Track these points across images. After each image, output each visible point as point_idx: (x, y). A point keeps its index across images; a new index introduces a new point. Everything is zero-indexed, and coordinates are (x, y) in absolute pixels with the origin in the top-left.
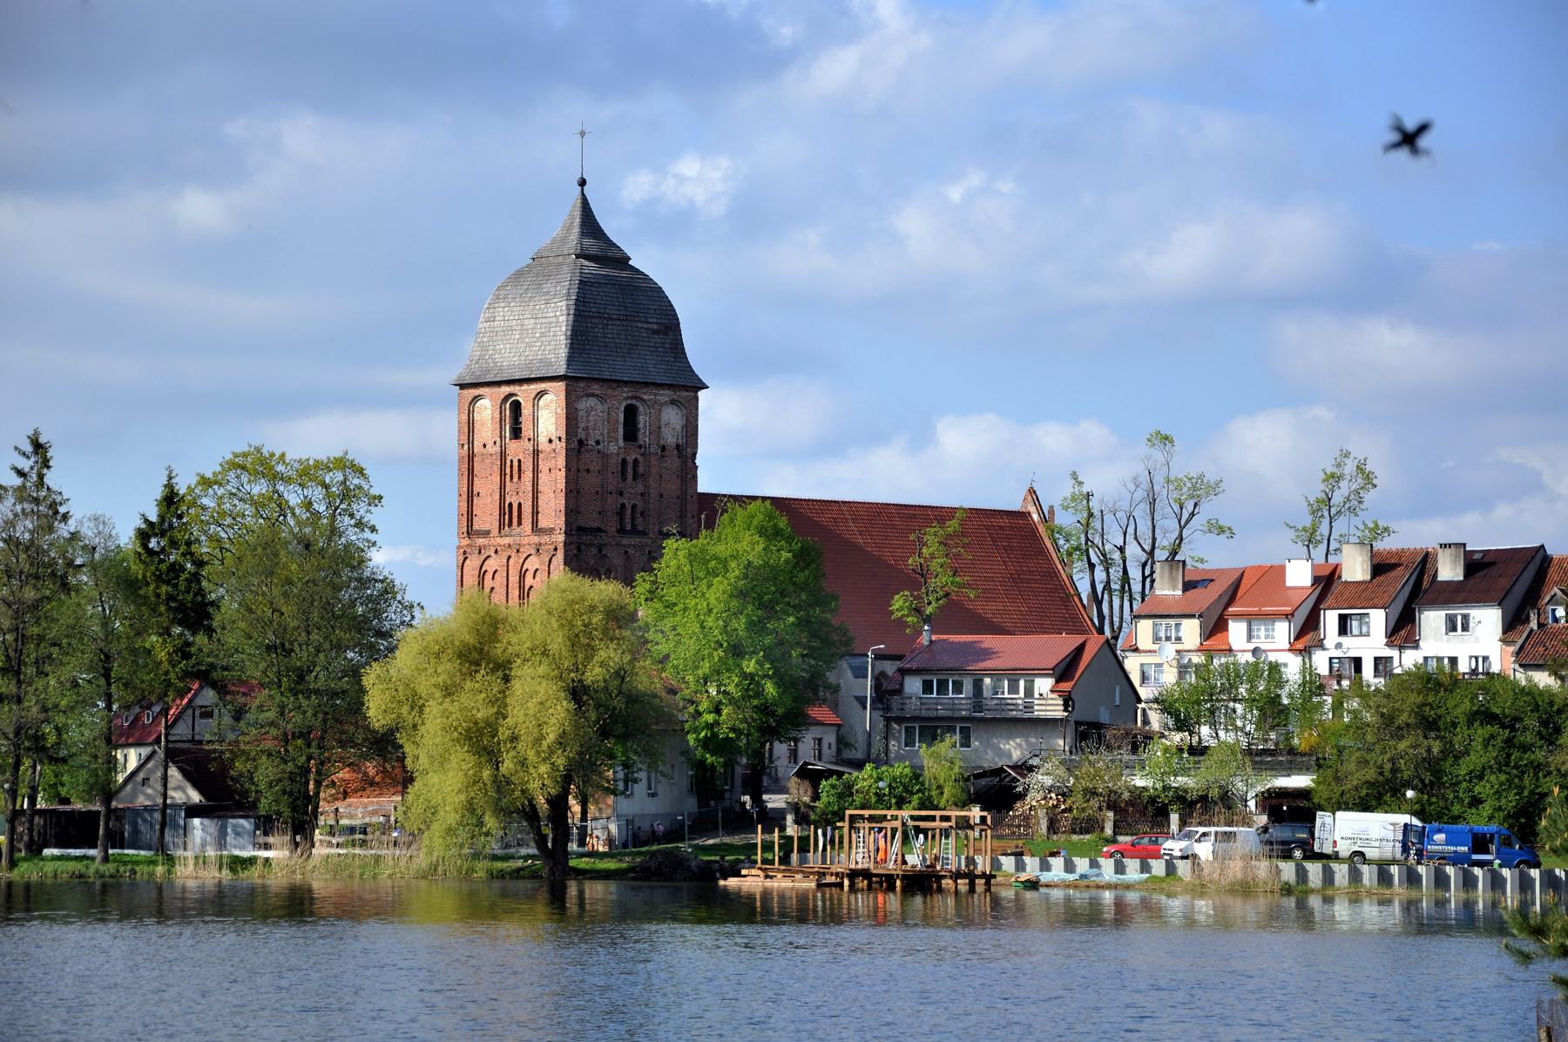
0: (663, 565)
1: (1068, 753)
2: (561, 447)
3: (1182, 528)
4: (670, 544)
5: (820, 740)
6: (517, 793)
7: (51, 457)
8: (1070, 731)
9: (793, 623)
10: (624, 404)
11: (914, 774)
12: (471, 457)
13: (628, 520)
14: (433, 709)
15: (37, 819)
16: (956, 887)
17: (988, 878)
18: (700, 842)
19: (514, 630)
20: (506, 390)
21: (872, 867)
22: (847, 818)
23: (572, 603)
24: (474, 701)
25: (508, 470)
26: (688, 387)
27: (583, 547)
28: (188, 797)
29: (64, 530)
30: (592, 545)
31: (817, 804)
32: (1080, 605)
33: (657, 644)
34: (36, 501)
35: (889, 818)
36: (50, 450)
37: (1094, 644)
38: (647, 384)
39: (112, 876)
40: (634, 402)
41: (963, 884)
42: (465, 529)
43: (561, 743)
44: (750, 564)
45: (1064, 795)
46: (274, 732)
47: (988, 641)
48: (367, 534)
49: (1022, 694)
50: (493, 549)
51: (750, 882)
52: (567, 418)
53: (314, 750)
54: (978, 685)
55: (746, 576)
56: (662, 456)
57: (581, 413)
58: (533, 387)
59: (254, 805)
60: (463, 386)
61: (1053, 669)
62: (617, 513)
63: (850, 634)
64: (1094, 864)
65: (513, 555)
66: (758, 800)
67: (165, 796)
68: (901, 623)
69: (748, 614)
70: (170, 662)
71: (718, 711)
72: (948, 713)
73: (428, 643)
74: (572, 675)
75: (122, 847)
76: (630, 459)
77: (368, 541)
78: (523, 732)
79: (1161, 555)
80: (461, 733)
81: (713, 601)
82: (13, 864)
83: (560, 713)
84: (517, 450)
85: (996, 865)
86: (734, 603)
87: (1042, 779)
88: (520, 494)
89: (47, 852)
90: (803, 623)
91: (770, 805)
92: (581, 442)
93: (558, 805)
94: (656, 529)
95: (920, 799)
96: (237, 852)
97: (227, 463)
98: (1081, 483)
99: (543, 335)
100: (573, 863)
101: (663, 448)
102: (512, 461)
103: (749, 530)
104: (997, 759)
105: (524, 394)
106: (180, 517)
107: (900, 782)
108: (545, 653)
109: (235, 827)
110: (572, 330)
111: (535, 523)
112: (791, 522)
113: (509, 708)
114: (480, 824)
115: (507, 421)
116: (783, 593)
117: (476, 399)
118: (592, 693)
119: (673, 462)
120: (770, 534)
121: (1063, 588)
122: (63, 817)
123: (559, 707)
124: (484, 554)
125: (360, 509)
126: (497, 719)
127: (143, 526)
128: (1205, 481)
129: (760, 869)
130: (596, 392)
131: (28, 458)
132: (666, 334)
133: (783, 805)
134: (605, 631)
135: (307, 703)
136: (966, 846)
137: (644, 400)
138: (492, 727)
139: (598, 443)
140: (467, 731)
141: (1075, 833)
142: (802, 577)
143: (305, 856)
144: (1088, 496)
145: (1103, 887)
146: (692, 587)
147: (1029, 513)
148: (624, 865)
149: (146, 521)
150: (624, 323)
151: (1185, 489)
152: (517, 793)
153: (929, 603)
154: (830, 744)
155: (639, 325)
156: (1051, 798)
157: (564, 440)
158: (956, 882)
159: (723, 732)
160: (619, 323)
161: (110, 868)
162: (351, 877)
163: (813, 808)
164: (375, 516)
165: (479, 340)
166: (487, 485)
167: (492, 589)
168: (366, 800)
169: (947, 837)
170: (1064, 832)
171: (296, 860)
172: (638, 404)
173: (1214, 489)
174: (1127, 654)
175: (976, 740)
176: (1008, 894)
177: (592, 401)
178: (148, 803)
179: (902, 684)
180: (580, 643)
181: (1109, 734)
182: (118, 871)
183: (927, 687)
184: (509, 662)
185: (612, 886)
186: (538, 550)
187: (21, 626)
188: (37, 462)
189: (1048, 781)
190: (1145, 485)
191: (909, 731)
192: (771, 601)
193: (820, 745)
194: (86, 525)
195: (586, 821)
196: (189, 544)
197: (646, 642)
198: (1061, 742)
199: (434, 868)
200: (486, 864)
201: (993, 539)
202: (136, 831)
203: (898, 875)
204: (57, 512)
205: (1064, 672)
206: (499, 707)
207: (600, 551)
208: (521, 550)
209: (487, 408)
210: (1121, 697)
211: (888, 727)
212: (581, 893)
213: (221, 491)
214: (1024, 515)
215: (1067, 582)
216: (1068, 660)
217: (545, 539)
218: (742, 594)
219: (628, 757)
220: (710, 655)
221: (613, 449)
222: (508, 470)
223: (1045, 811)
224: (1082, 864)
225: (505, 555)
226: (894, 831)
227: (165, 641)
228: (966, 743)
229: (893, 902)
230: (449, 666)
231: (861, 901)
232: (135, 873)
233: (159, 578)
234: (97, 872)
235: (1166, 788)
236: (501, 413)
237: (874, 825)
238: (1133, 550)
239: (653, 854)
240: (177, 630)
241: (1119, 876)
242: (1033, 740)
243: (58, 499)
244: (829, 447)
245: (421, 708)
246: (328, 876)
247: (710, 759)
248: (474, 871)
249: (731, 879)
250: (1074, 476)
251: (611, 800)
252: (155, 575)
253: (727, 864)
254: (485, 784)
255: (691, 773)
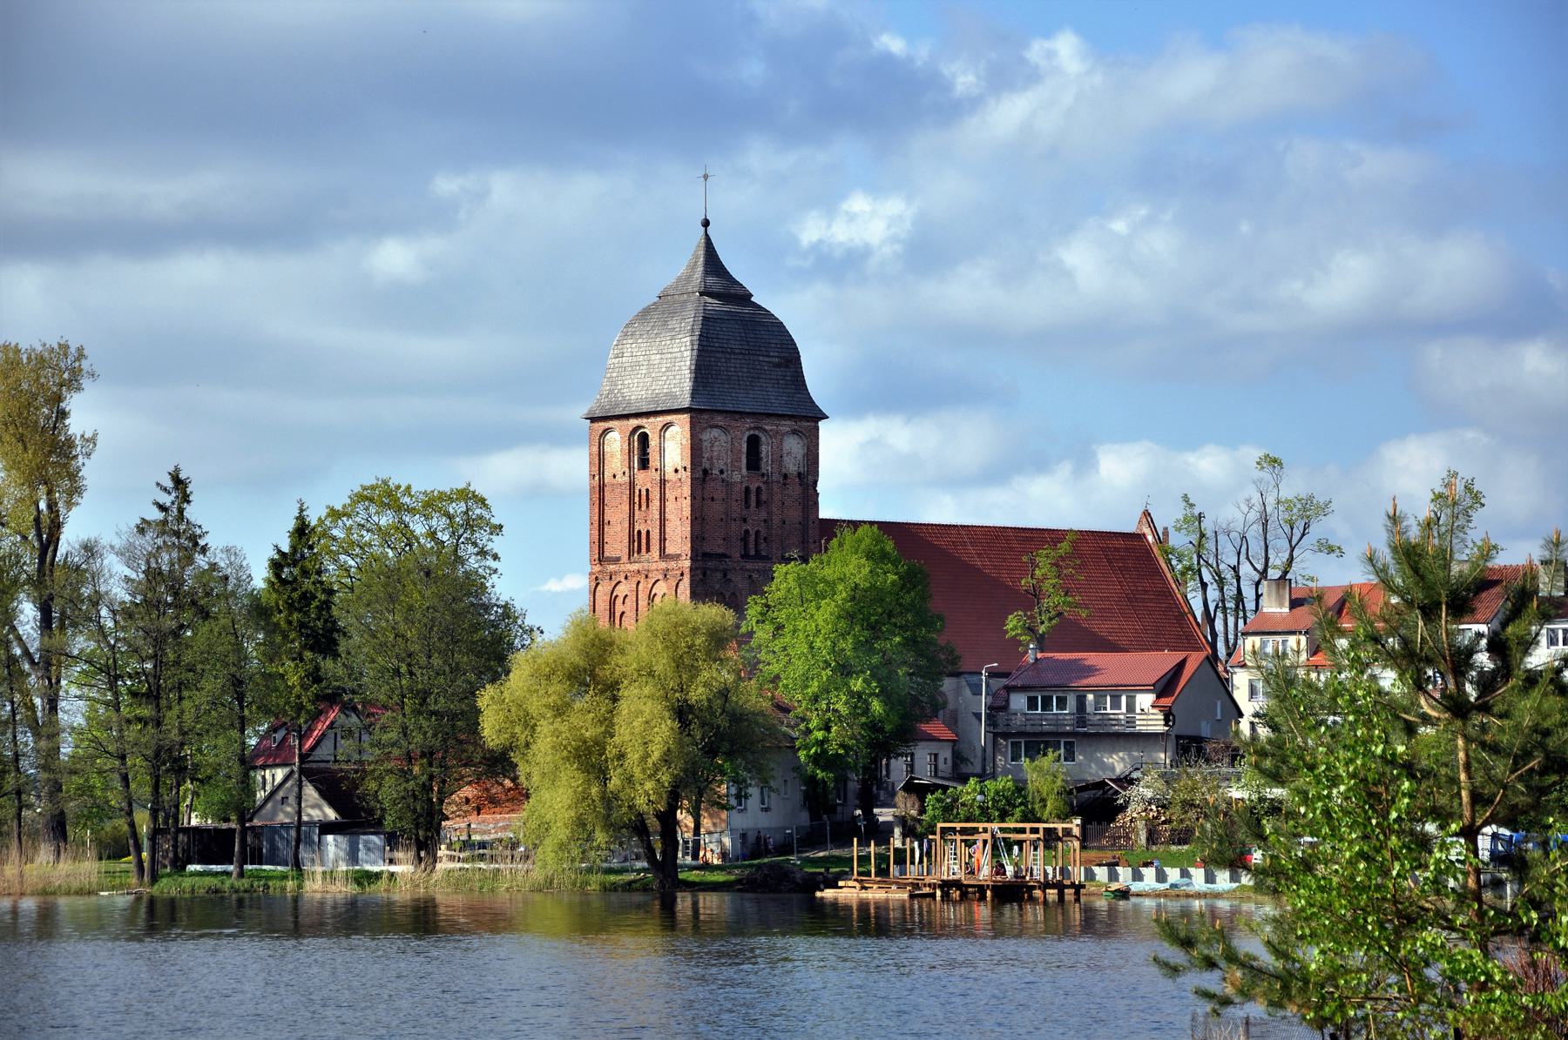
0: (774, 588)
1: (1169, 766)
2: (686, 476)
3: (1292, 551)
4: (780, 570)
5: (936, 755)
6: (624, 810)
7: (191, 492)
8: (1171, 746)
9: (899, 642)
10: (747, 434)
11: (1017, 787)
12: (602, 487)
13: (752, 546)
14: (544, 728)
15: (181, 836)
16: (1045, 897)
17: (1078, 888)
18: (811, 855)
19: (622, 652)
20: (634, 422)
21: (963, 879)
22: (938, 831)
23: (676, 625)
24: (583, 720)
25: (637, 499)
26: (808, 417)
27: (708, 572)
28: (325, 815)
29: (201, 561)
30: (717, 570)
31: (923, 817)
32: (1194, 623)
33: (769, 664)
34: (177, 534)
35: (981, 830)
36: (190, 486)
37: (1195, 660)
38: (769, 415)
39: (246, 891)
40: (756, 432)
41: (1052, 894)
42: (597, 556)
43: (666, 761)
44: (856, 585)
45: (1164, 806)
46: (396, 752)
47: (1092, 658)
48: (490, 562)
49: (1124, 709)
50: (623, 575)
51: (847, 893)
52: (692, 448)
53: (435, 770)
54: (1081, 701)
55: (853, 598)
56: (784, 484)
57: (705, 444)
58: (600, 424)
59: (379, 823)
60: (593, 420)
61: (1153, 685)
62: (741, 539)
63: (956, 653)
64: (1185, 874)
65: (642, 581)
66: (868, 814)
67: (299, 813)
68: (1015, 642)
69: (854, 635)
70: (302, 686)
71: (828, 729)
72: (1052, 729)
73: (540, 665)
74: (677, 695)
75: (261, 864)
76: (753, 487)
77: (489, 568)
78: (629, 750)
79: (1274, 574)
80: (570, 752)
81: (821, 623)
82: (155, 879)
83: (664, 731)
84: (644, 480)
85: (1090, 876)
86: (842, 624)
87: (1144, 791)
88: (648, 522)
89: (191, 868)
90: (911, 643)
91: (881, 819)
92: (705, 472)
93: (668, 822)
94: (779, 554)
95: (1023, 811)
96: (368, 867)
97: (356, 495)
98: (1192, 505)
99: (668, 369)
100: (682, 876)
101: (785, 476)
102: (640, 491)
103: (856, 553)
104: (1101, 773)
105: (651, 426)
106: (311, 547)
107: (1003, 795)
108: (651, 674)
109: (366, 842)
110: (696, 365)
111: (662, 549)
112: (898, 545)
113: (616, 727)
114: (589, 839)
115: (636, 453)
116: (890, 615)
117: (606, 431)
118: (697, 712)
119: (795, 490)
120: (877, 557)
121: (1177, 606)
122: (205, 835)
123: (663, 726)
124: (615, 579)
125: (482, 537)
126: (604, 737)
127: (276, 557)
128: (1315, 502)
129: (856, 880)
130: (720, 424)
131: (169, 493)
132: (787, 367)
133: (890, 818)
134: (708, 653)
135: (428, 724)
136: (1055, 857)
137: (766, 431)
138: (600, 745)
139: (722, 472)
140: (576, 749)
141: (1173, 844)
142: (907, 599)
143: (428, 871)
144: (1200, 517)
145: (1192, 896)
146: (801, 609)
147: (1144, 535)
148: (732, 878)
149: (279, 551)
150: (747, 357)
151: (1295, 510)
152: (624, 810)
153: (1042, 623)
154: (946, 759)
155: (761, 358)
156: (1151, 810)
157: (689, 470)
158: (1044, 892)
159: (833, 748)
160: (741, 357)
161: (245, 883)
162: (471, 890)
163: (920, 821)
164: (496, 544)
165: (609, 375)
166: (617, 514)
167: (623, 613)
168: (498, 816)
169: (1035, 849)
170: (1162, 843)
171: (420, 874)
172: (761, 435)
173: (1324, 509)
174: (1236, 670)
175: (1080, 754)
176: (1101, 904)
177: (716, 432)
178: (287, 821)
179: (1007, 701)
180: (685, 665)
181: (1208, 748)
182: (252, 886)
183: (1032, 703)
184: (617, 683)
185: (727, 897)
186: (665, 575)
187: (159, 653)
188: (177, 497)
189: (1149, 794)
190: (1258, 507)
191: (1015, 745)
192: (876, 621)
193: (936, 760)
194: (219, 556)
195: (699, 835)
196: (319, 573)
197: (759, 662)
198: (1162, 756)
199: (549, 882)
200: (600, 877)
201: (1110, 561)
202: (273, 848)
203: (988, 886)
204: (196, 544)
205: (1165, 687)
206: (607, 726)
207: (725, 576)
208: (650, 575)
209: (616, 442)
210: (1222, 709)
211: (995, 743)
212: (695, 905)
213: (349, 523)
214: (1140, 537)
215: (1182, 601)
216: (1169, 676)
217: (673, 564)
218: (850, 617)
219: (737, 773)
220: (819, 675)
221: (736, 477)
222: (637, 499)
223: (1144, 822)
224: (1173, 874)
225: (634, 580)
226: (985, 842)
227: (297, 665)
228: (1070, 756)
229: (983, 912)
230: (559, 687)
231: (953, 913)
232: (268, 888)
233: (291, 607)
234: (232, 888)
235: (1262, 800)
236: (629, 444)
237: (965, 837)
238: (1245, 569)
239: (759, 867)
240: (308, 655)
241: (1209, 885)
242: (1136, 754)
243: (198, 531)
244: (995, 474)
245: (533, 728)
246: (449, 890)
247: (820, 774)
248: (588, 883)
249: (827, 891)
250: (1186, 498)
251: (724, 814)
252: (287, 603)
253: (830, 876)
254: (593, 801)
255: (803, 788)
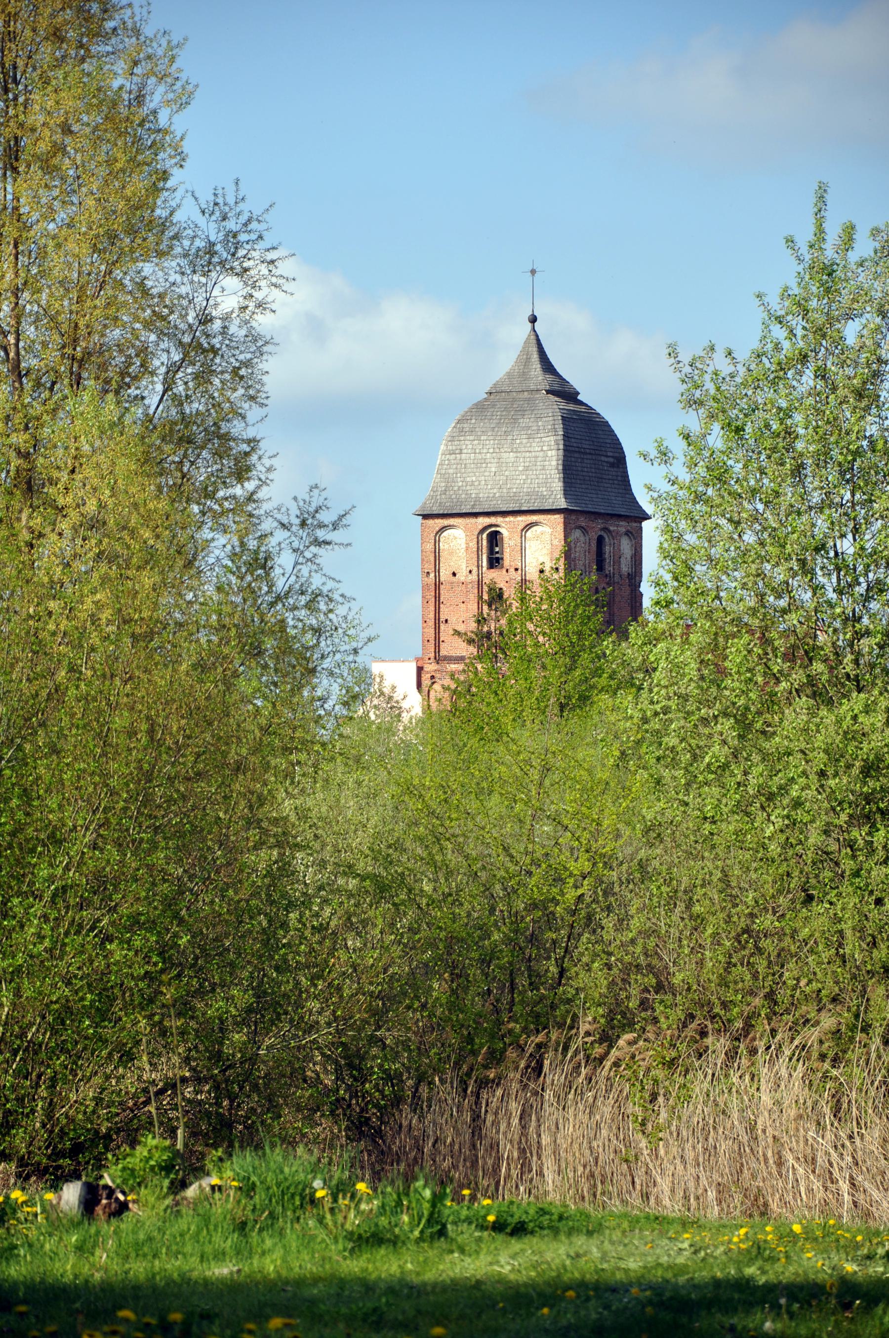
20: (484, 521)
38: (612, 516)
58: (437, 521)
60: (426, 517)
117: (443, 529)
119: (626, 591)
137: (610, 531)
172: (605, 535)
